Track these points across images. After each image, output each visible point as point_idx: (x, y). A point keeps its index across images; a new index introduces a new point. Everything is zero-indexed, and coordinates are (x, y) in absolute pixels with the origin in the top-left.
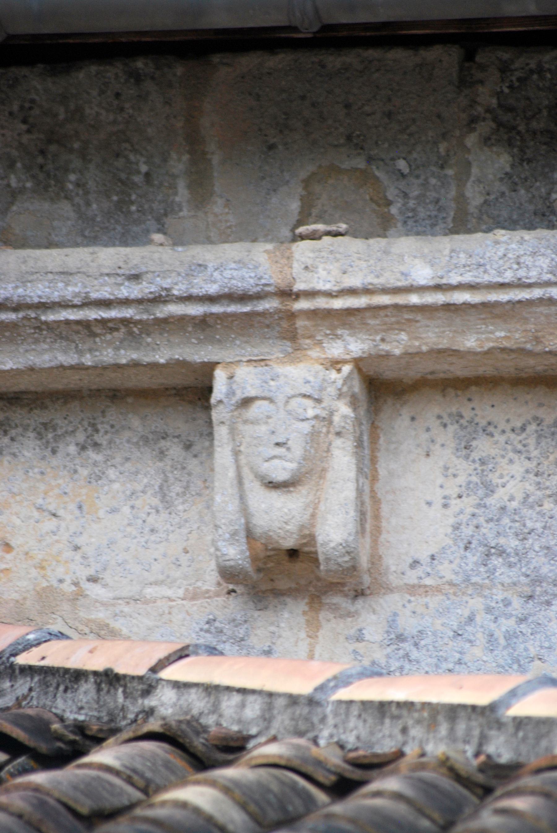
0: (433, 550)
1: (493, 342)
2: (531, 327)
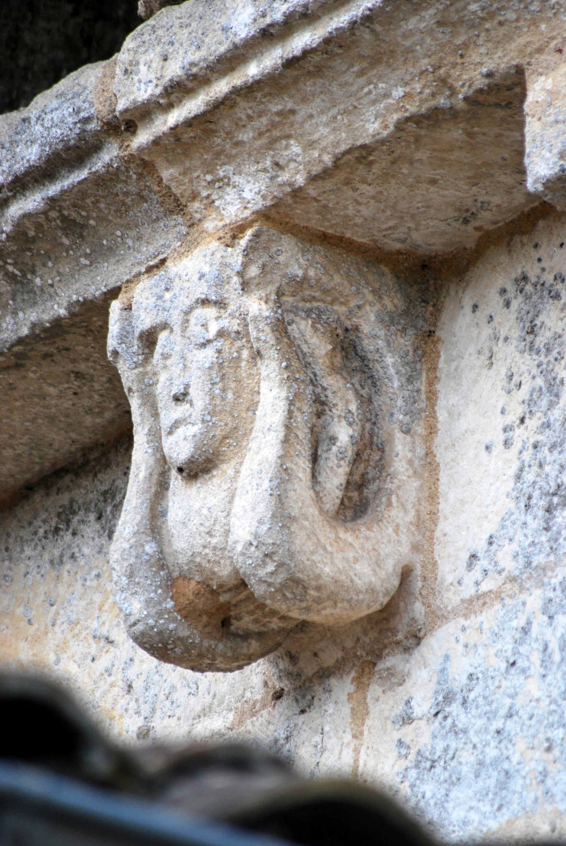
0: (490, 528)
1: (396, 111)
2: (424, 63)
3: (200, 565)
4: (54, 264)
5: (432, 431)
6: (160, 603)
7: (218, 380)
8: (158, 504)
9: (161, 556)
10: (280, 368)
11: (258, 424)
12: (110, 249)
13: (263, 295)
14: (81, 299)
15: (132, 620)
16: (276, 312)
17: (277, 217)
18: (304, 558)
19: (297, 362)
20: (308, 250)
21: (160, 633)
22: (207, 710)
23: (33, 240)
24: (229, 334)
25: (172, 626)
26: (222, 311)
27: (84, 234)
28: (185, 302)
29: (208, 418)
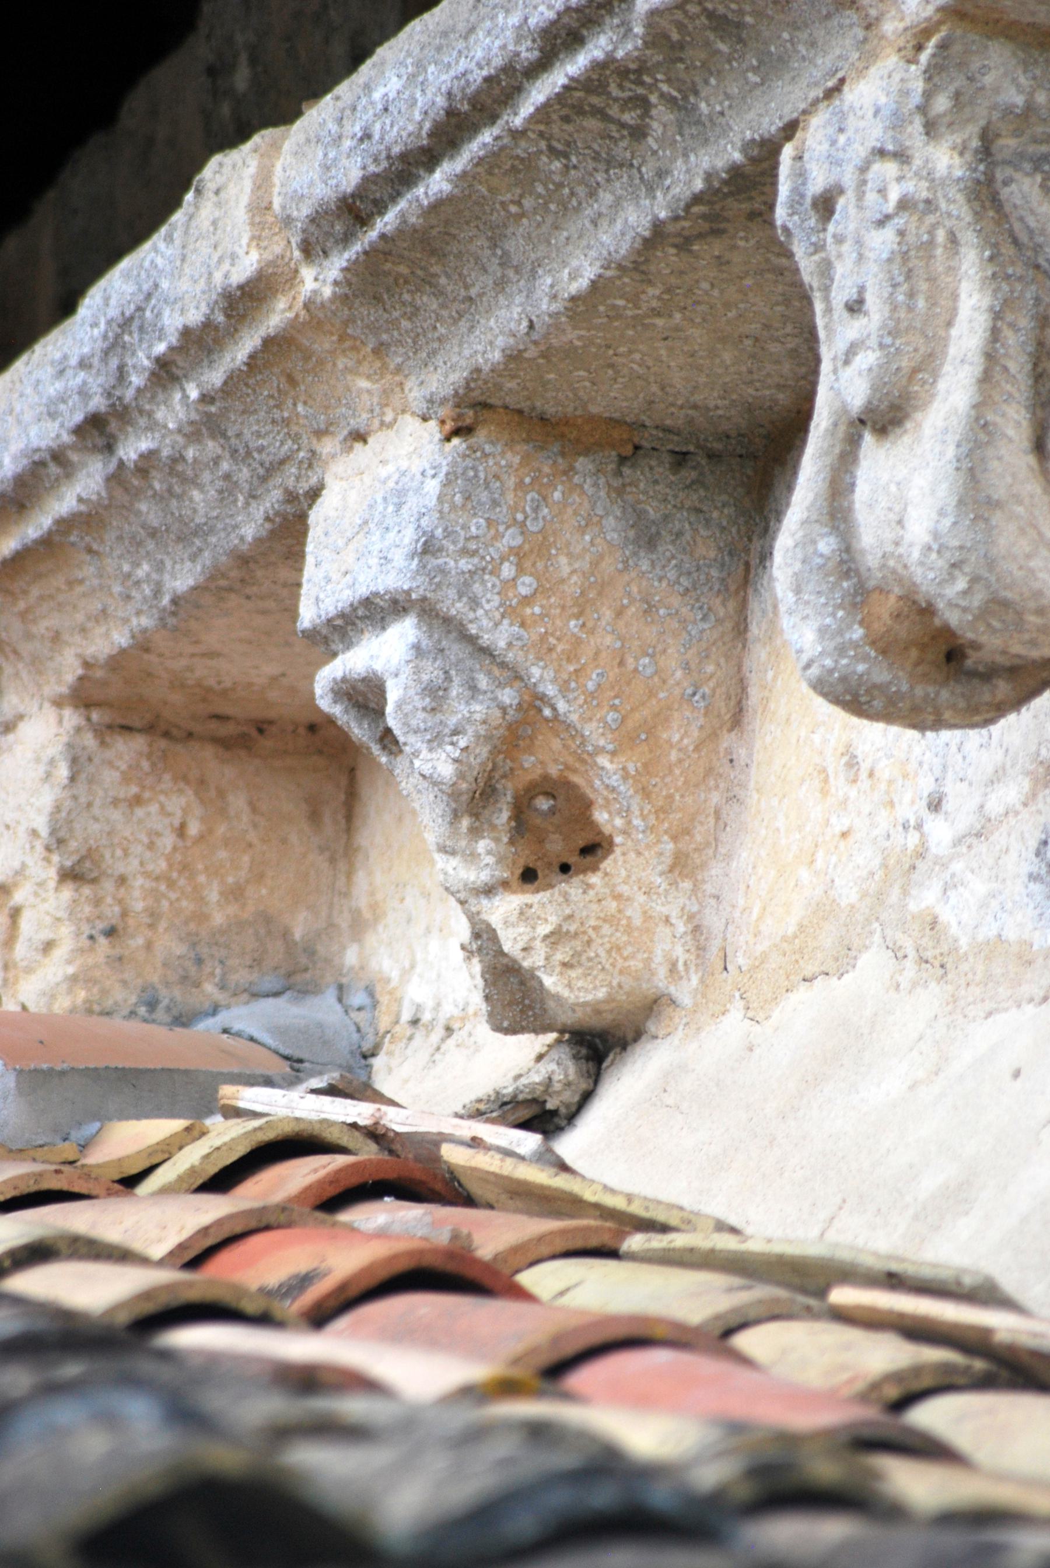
3: (894, 572)
4: (719, 82)
6: (840, 632)
7: (901, 279)
8: (846, 471)
9: (845, 556)
10: (982, 259)
11: (952, 351)
12: (780, 59)
13: (959, 141)
14: (757, 137)
15: (805, 658)
16: (975, 170)
18: (1014, 567)
20: (1036, 62)
21: (843, 679)
22: (1001, 772)
23: (681, 46)
24: (915, 205)
25: (861, 668)
26: (905, 167)
27: (744, 36)
28: (859, 151)
29: (888, 340)
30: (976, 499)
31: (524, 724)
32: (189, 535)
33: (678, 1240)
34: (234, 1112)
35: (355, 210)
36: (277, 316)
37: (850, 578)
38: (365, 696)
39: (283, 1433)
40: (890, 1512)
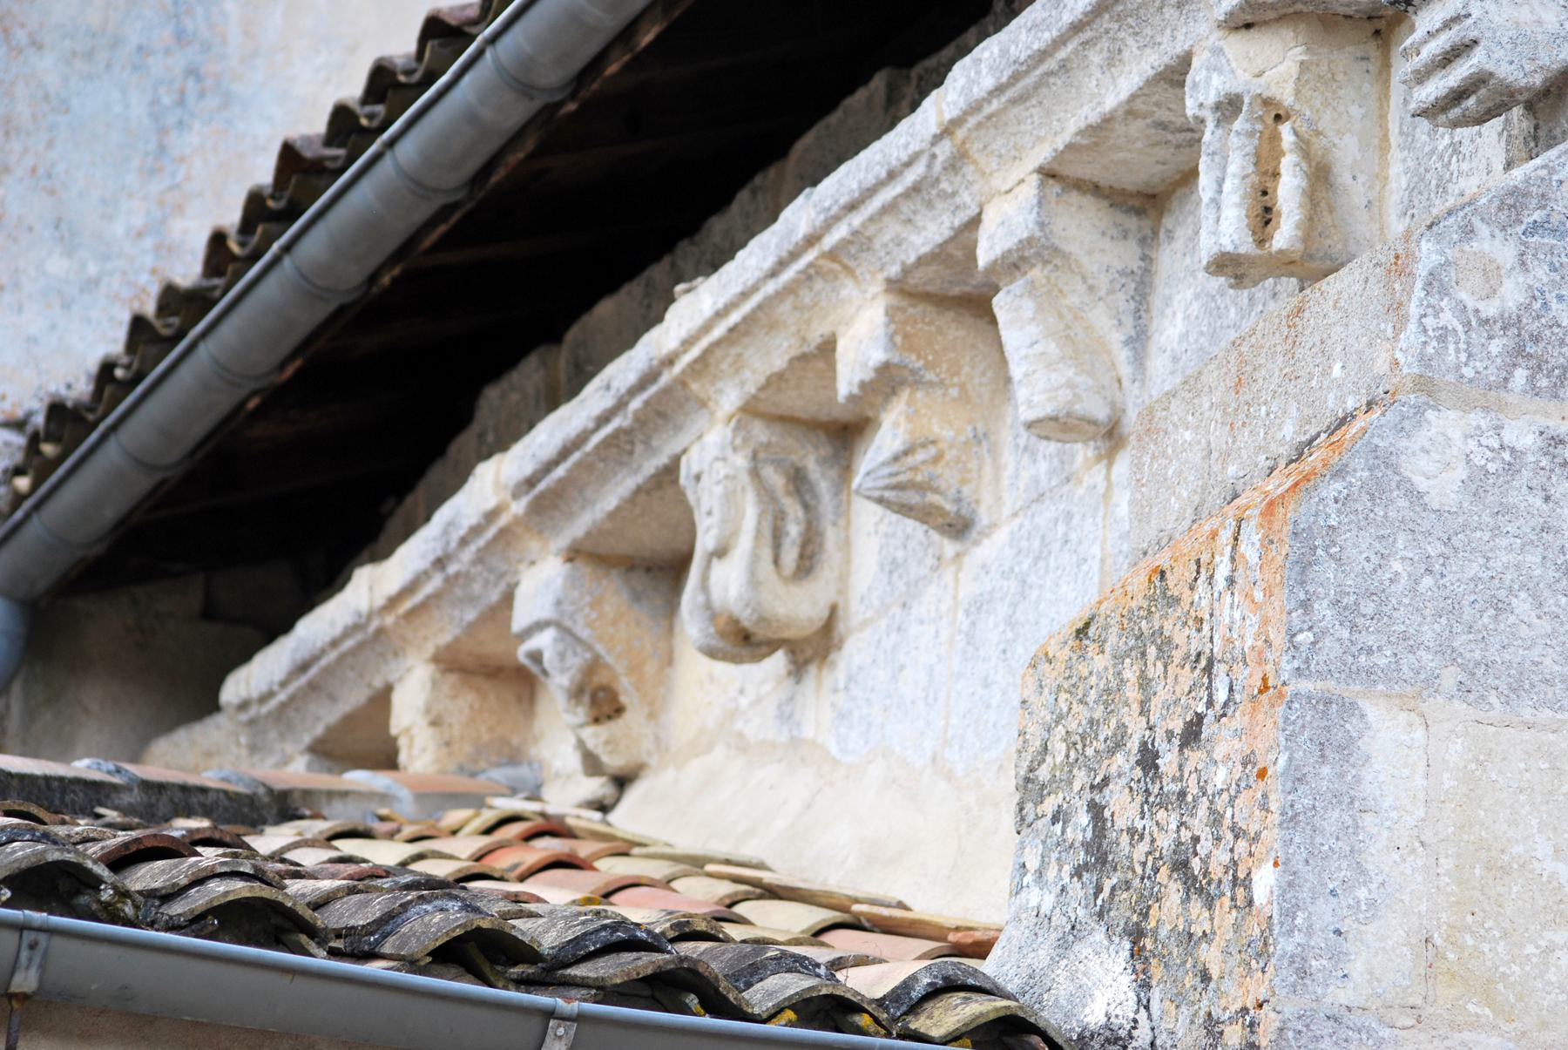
5: (849, 523)
17: (750, 409)
19: (766, 494)
30: (753, 581)
31: (594, 666)
32: (471, 600)
33: (651, 850)
34: (491, 807)
35: (530, 482)
36: (503, 520)
37: (710, 612)
38: (536, 656)
39: (506, 916)
40: (727, 940)
